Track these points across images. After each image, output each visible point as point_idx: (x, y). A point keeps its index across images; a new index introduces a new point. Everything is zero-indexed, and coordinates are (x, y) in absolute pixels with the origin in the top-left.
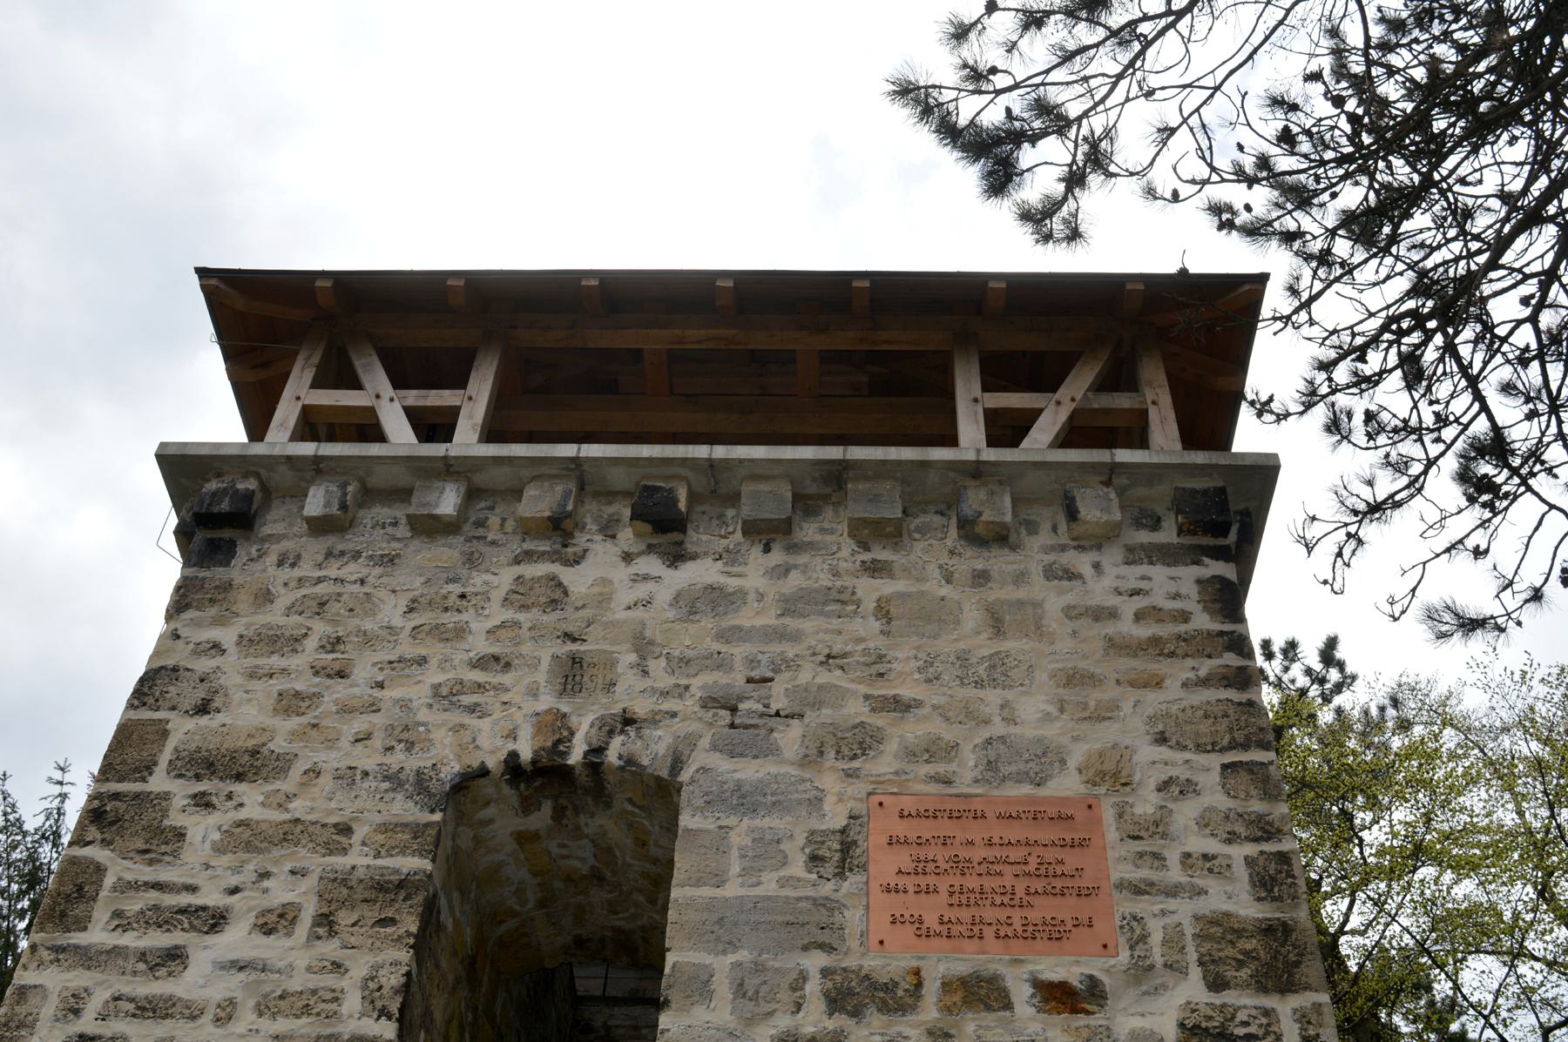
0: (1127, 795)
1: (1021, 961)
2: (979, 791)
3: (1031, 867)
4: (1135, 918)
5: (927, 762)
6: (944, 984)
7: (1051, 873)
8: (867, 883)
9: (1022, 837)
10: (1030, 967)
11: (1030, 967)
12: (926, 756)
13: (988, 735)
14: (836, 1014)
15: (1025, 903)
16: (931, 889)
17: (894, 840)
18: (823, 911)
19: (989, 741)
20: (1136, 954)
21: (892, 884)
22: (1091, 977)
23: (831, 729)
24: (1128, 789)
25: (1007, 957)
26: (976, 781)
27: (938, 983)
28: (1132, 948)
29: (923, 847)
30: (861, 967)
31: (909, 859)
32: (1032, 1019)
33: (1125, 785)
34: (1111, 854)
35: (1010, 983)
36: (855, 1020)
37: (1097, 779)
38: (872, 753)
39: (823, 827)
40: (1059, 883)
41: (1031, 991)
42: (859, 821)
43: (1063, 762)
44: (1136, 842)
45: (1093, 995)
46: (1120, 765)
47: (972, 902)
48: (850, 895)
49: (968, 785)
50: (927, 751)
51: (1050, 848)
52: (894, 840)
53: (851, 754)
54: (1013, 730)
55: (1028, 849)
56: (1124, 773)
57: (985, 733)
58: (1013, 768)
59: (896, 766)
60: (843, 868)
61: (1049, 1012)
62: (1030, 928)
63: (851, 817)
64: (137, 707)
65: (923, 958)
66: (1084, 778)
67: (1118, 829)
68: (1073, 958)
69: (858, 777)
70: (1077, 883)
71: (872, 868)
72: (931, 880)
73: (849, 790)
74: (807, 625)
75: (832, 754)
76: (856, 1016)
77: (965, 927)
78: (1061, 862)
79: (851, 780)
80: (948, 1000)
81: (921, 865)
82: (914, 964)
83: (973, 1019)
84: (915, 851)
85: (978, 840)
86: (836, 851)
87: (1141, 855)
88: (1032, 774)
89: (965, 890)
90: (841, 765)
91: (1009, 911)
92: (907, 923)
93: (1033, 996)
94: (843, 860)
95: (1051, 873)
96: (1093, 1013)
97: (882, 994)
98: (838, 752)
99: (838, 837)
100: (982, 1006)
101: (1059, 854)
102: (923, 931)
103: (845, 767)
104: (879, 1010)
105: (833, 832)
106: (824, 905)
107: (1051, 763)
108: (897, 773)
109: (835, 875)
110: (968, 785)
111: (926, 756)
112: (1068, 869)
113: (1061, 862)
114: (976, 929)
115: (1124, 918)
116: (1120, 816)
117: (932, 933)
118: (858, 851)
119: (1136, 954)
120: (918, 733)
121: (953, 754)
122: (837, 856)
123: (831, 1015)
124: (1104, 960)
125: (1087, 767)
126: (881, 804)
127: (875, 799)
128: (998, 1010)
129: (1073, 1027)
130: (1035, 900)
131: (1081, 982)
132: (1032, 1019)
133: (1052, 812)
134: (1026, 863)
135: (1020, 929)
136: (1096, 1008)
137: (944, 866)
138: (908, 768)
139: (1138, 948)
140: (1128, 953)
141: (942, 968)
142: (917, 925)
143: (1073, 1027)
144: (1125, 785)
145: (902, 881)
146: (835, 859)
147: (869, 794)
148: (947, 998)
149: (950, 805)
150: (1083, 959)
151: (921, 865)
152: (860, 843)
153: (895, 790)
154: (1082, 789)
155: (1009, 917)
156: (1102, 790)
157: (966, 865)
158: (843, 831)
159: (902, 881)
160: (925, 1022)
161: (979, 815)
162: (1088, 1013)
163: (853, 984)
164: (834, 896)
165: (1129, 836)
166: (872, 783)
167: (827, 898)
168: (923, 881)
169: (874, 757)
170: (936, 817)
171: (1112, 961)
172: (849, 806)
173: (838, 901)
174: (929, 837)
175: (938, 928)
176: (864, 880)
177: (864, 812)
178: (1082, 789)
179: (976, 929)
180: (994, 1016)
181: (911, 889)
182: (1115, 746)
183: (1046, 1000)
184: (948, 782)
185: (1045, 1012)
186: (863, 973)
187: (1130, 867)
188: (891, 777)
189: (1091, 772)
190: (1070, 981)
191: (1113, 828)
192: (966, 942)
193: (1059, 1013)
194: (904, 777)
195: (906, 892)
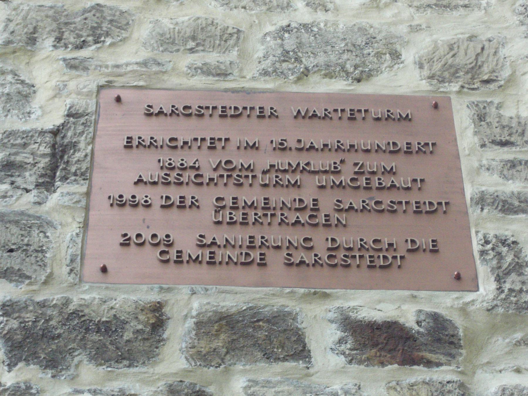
0: (492, 93)
1: (326, 296)
2: (270, 86)
3: (345, 178)
4: (504, 242)
5: (192, 51)
6: (199, 324)
7: (375, 183)
8: (88, 194)
9: (332, 141)
10: (338, 304)
11: (338, 304)
12: (191, 44)
13: (285, 23)
14: (21, 365)
15: (334, 222)
16: (188, 202)
17: (135, 143)
18: (14, 229)
19: (287, 29)
20: (507, 286)
21: (127, 196)
22: (436, 317)
23: (51, 13)
24: (492, 86)
25: (302, 291)
26: (265, 73)
27: (190, 323)
28: (499, 279)
29: (179, 151)
30: (67, 302)
31: (157, 166)
32: (339, 372)
33: (487, 82)
34: (465, 165)
35: (303, 323)
36: (50, 373)
37: (446, 74)
38: (109, 41)
39: (27, 127)
40: (386, 198)
41: (339, 334)
42: (83, 120)
43: (396, 56)
44: (506, 149)
45: (439, 340)
46: (480, 59)
47: (251, 218)
48: (56, 209)
49: (253, 78)
50: (194, 38)
51: (373, 155)
52: (135, 143)
53: (79, 41)
54: (321, 16)
55: (341, 156)
56: (486, 69)
57: (282, 20)
58: (321, 59)
59: (144, 54)
60: (53, 177)
61: (369, 361)
62: (341, 254)
63: (69, 115)
64: (418, 316)
65: (169, 290)
66: (426, 72)
67: (476, 133)
68: (407, 293)
69: (86, 69)
70: (413, 197)
71: (97, 178)
72: (189, 192)
73: (72, 85)
74: (440, 65)
75: (49, 42)
76: (54, 367)
77: (237, 251)
78: (391, 172)
79: (74, 72)
80: (204, 346)
81: (174, 174)
82: (154, 297)
83: (244, 372)
84: (166, 156)
85: (265, 144)
86: (44, 155)
87: (513, 164)
88: (349, 67)
89: (241, 204)
90: (61, 53)
91: (308, 232)
92: (147, 246)
93: (341, 341)
94: (54, 168)
95: (375, 183)
96: (439, 365)
97: (95, 337)
98: (59, 39)
99: (48, 138)
100: (259, 355)
101: (389, 162)
102: (173, 255)
103: (69, 56)
104: (92, 358)
105: (42, 133)
106: (17, 222)
107: (379, 55)
108: (145, 64)
109: (38, 186)
110: (253, 78)
111: (191, 44)
112: (400, 181)
113: (391, 172)
114: (255, 255)
115: (487, 242)
116: (481, 117)
117: (185, 258)
118: (79, 155)
119: (507, 286)
120: (181, 19)
121: (231, 42)
122: (44, 162)
123: (11, 366)
124: (455, 295)
125: (430, 61)
126: (118, 99)
127: (110, 94)
128: (285, 360)
129: (404, 383)
130: (354, 219)
131: (418, 323)
132: (339, 372)
133: (379, 111)
134: (337, 172)
135: (324, 255)
136: (443, 359)
137: (207, 174)
138: (165, 58)
139: (509, 280)
140: (493, 286)
141: (196, 305)
142: (162, 248)
143: (404, 383)
144: (487, 82)
145: (141, 193)
146: (41, 165)
147: (100, 88)
148: (203, 343)
149: (230, 102)
150: (423, 294)
151: (174, 174)
152: (82, 145)
153: (141, 83)
154: (424, 86)
155: (306, 240)
156: (455, 87)
157: (244, 173)
158: (55, 132)
159: (141, 193)
160: (165, 375)
161: (267, 112)
162: (429, 364)
163: (53, 323)
164: (34, 210)
165: (493, 142)
166: (108, 75)
167: (22, 213)
168: (175, 193)
169: (112, 45)
170: (201, 116)
171: (469, 297)
172: (68, 101)
173: (39, 218)
174: (188, 139)
175: (195, 252)
176: (84, 189)
177: (92, 108)
178: (424, 86)
179: (255, 255)
180: (278, 367)
181: (157, 203)
182: (472, 38)
183: (360, 346)
184: (223, 74)
185: (360, 362)
186: (72, 308)
187: (496, 177)
188: (135, 67)
189: (437, 67)
190: (402, 321)
191: (470, 132)
192: (239, 272)
193: (382, 364)
194: (155, 68)
195: (148, 206)
